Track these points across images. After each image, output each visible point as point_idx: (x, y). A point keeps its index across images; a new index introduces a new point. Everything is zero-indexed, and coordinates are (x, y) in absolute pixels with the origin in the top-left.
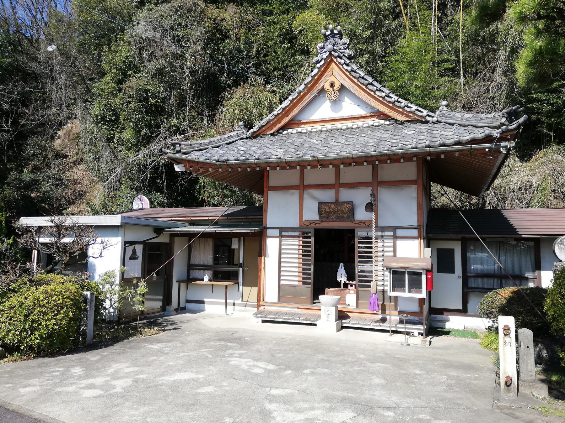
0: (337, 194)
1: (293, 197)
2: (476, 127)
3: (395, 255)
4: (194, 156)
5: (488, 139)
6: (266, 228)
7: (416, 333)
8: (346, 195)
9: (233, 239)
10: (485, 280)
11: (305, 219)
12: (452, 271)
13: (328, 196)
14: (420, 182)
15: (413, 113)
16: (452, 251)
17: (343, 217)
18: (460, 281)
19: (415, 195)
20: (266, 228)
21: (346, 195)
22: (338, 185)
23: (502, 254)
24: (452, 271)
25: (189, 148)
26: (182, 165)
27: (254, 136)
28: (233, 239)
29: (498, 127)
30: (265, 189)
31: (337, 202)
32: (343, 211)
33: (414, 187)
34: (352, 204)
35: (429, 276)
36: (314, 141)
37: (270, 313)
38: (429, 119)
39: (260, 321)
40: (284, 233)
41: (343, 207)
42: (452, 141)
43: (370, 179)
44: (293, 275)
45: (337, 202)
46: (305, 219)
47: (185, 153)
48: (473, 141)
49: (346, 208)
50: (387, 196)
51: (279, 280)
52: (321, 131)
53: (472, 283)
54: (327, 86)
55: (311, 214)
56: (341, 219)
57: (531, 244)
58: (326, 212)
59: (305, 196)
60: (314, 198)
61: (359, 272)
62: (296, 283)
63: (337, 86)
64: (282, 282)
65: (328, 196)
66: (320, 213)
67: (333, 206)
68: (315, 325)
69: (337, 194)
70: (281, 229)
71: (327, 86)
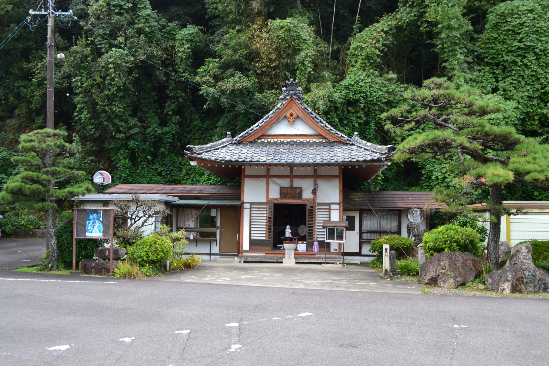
0: (291, 182)
1: (262, 183)
2: (373, 152)
3: (330, 220)
4: (205, 156)
5: (379, 160)
6: (243, 203)
7: (338, 263)
8: (297, 183)
9: (212, 210)
10: (372, 234)
11: (270, 197)
12: (354, 230)
13: (285, 183)
14: (341, 177)
15: (340, 138)
16: (354, 217)
17: (295, 197)
18: (358, 235)
19: (338, 184)
20: (243, 203)
21: (297, 183)
22: (292, 177)
23: (392, 222)
24: (354, 230)
25: (201, 150)
26: (196, 161)
27: (239, 143)
28: (212, 210)
29: (384, 154)
30: (243, 177)
31: (291, 187)
32: (295, 193)
33: (338, 179)
34: (301, 188)
35: (515, 211)
36: (281, 150)
37: (248, 257)
38: (348, 142)
39: (243, 262)
40: (253, 206)
41: (296, 191)
42: (362, 159)
43: (312, 174)
44: (261, 234)
45: (291, 187)
46: (270, 197)
47: (198, 154)
48: (372, 161)
49: (298, 191)
50: (322, 185)
51: (250, 236)
52: (283, 142)
53: (365, 236)
54: (288, 115)
55: (275, 194)
56: (294, 198)
57: (397, 212)
58: (285, 193)
59: (270, 182)
60: (276, 184)
61: (214, 235)
62: (264, 238)
63: (295, 116)
64: (252, 238)
65: (285, 183)
66: (281, 194)
67: (289, 189)
68: (282, 262)
69: (291, 182)
70: (251, 204)
71: (288, 115)
